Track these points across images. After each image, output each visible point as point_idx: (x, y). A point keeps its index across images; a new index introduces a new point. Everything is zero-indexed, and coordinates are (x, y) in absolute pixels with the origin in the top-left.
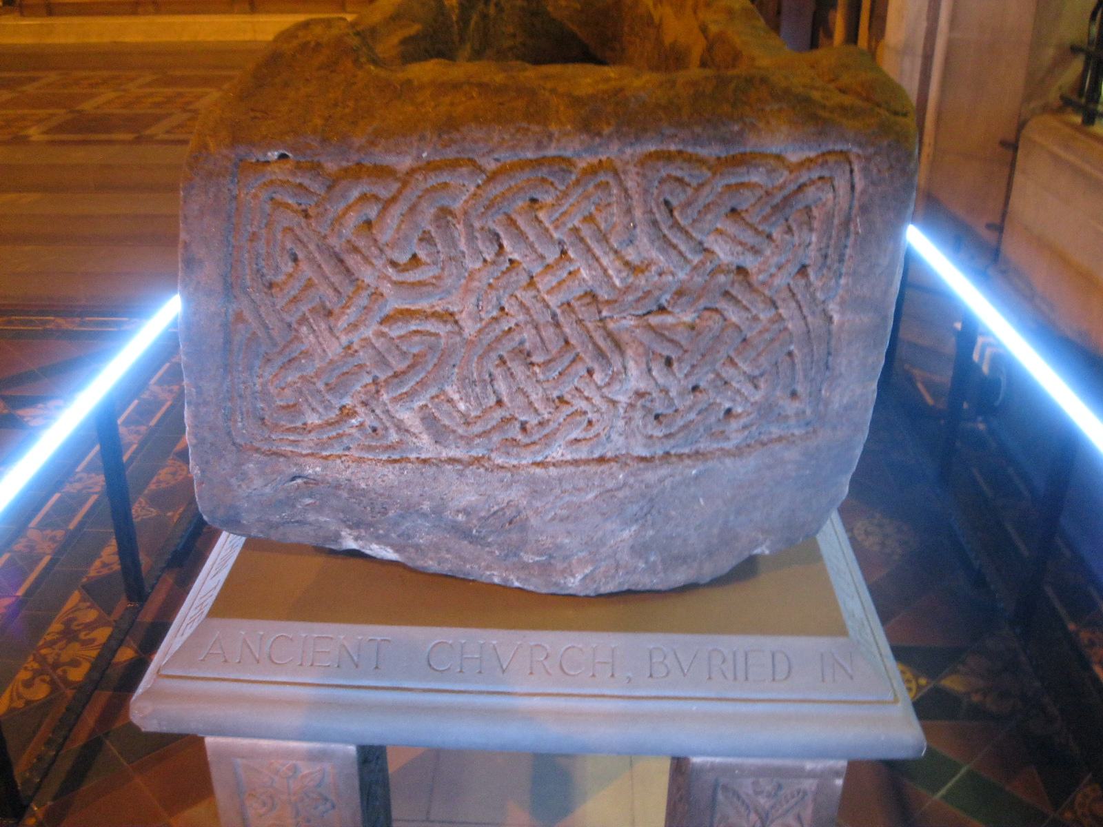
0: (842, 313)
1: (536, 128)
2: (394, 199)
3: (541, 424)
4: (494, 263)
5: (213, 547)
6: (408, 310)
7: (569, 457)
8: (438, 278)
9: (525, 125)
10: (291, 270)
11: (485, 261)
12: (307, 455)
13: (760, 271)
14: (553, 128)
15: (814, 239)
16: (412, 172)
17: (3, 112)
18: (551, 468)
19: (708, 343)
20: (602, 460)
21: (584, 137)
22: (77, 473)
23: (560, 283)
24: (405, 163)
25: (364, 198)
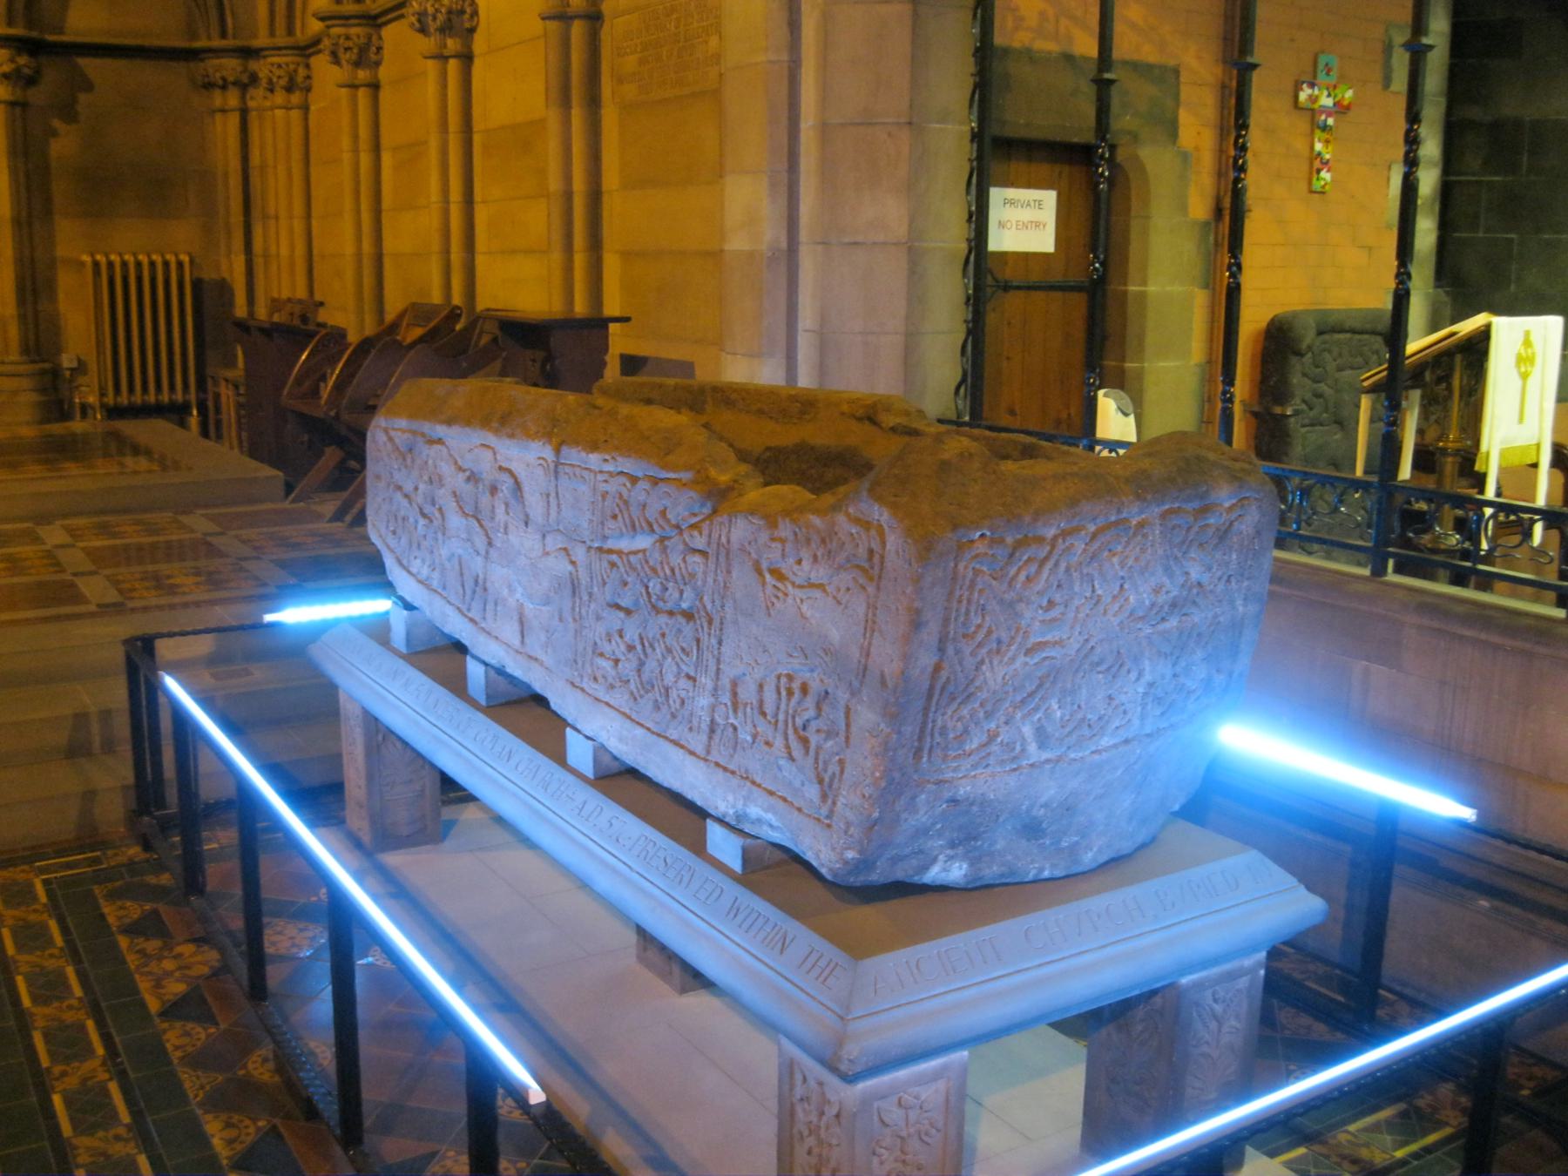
0: (1245, 606)
1: (1115, 500)
2: (1046, 559)
3: (1100, 718)
4: (1091, 598)
5: (1341, 1062)
6: (1041, 642)
7: (1111, 743)
8: (1063, 614)
9: (1109, 499)
10: (979, 621)
11: (1086, 598)
12: (961, 778)
13: (1210, 584)
14: (1124, 498)
15: (1234, 556)
16: (1055, 538)
17: (5, 873)
18: (1104, 753)
19: (859, 662)
20: (1127, 741)
21: (1138, 503)
22: (1529, 1089)
23: (1120, 608)
24: (1050, 532)
25: (1029, 560)
